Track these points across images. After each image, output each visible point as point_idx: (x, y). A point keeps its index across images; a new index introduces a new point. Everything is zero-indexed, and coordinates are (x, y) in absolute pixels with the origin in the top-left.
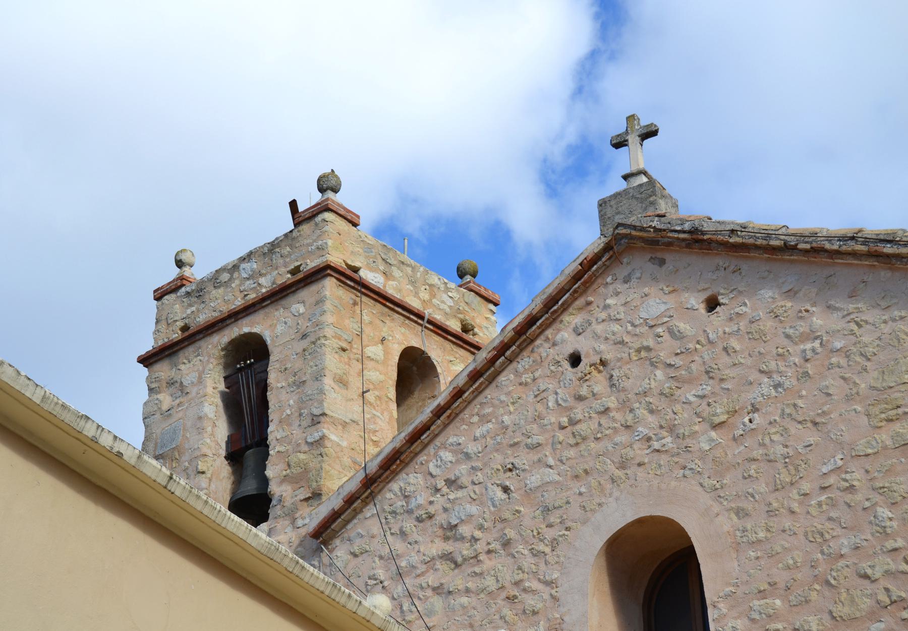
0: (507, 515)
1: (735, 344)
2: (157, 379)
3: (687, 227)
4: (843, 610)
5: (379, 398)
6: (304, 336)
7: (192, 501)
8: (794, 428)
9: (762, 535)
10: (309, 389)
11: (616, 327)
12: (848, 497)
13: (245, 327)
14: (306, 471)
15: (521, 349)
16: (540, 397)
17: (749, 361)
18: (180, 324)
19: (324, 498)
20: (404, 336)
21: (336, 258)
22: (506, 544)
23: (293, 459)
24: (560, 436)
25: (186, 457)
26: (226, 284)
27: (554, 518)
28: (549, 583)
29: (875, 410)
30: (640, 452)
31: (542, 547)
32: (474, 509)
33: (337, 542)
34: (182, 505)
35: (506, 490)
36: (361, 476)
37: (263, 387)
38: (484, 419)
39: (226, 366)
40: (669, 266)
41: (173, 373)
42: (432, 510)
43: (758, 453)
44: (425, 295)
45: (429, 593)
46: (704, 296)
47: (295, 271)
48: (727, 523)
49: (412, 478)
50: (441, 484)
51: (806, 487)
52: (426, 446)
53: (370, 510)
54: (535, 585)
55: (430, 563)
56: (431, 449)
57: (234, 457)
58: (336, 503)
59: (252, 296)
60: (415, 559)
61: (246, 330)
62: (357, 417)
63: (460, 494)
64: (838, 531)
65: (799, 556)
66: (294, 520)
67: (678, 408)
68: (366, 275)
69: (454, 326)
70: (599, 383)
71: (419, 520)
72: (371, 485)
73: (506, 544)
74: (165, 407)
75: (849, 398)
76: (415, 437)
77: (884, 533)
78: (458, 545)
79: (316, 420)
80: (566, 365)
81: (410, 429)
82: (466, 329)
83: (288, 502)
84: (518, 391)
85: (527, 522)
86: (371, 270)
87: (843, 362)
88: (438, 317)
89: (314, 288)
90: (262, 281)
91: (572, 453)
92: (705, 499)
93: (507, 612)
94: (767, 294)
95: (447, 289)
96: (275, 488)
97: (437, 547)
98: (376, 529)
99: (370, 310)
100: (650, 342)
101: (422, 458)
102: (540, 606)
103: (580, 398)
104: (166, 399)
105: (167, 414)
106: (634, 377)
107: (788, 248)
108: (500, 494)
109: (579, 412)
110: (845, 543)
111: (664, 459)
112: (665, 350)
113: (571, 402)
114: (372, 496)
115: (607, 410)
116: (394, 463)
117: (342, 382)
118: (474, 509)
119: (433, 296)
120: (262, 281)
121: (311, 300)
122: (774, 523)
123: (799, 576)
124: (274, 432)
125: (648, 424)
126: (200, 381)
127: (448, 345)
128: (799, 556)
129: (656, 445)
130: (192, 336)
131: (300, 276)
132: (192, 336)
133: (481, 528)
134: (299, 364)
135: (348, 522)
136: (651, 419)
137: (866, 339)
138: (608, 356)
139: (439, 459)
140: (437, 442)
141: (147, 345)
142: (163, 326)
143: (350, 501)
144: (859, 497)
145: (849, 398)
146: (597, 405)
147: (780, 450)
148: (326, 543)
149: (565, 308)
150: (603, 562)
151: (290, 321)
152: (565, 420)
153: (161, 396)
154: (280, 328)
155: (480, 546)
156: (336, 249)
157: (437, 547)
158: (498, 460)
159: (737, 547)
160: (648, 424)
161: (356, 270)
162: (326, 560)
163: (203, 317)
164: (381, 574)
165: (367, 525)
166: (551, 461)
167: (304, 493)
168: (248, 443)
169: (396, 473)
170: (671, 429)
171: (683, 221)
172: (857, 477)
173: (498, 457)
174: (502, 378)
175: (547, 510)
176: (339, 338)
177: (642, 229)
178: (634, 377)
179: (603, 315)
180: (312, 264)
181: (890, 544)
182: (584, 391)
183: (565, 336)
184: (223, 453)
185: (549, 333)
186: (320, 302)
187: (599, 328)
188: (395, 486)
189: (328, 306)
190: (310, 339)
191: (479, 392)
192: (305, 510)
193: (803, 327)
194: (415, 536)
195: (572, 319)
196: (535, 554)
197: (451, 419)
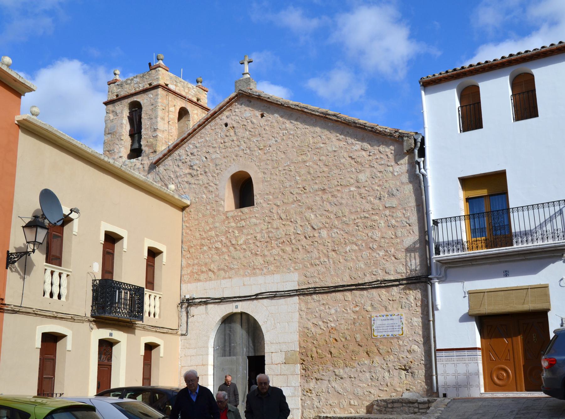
0: (206, 165)
1: (267, 128)
2: (109, 110)
3: (257, 94)
4: (285, 201)
5: (173, 123)
6: (152, 105)
7: (126, 171)
8: (279, 153)
9: (269, 179)
10: (154, 120)
11: (237, 118)
12: (290, 173)
13: (135, 99)
14: (152, 144)
15: (212, 120)
16: (216, 133)
17: (270, 133)
18: (116, 94)
19: (157, 153)
20: (181, 103)
21: (162, 82)
22: (205, 173)
23: (149, 140)
24: (221, 145)
25: (117, 135)
26: (130, 84)
27: (218, 168)
28: (215, 185)
29: (298, 151)
30: (241, 153)
31: (214, 175)
32: (197, 162)
33: (160, 166)
34: (124, 172)
35: (206, 158)
36: (168, 149)
37: (140, 118)
38: (201, 137)
39: (129, 109)
40: (252, 103)
41: (113, 109)
42: (186, 160)
43: (270, 158)
44: (187, 91)
45: (185, 183)
46: (261, 113)
47: (150, 84)
48: (261, 175)
49: (181, 151)
50: (189, 154)
51: (280, 169)
52: (185, 143)
53: (169, 158)
54: (212, 185)
55: (185, 175)
56: (187, 144)
57: (132, 135)
58: (161, 156)
59: (137, 90)
60: (182, 173)
61: (135, 99)
62: (167, 129)
63: (194, 157)
64: (287, 181)
65: (277, 186)
66: (149, 158)
67: (251, 143)
68: (171, 87)
69: (195, 100)
70: (232, 132)
71: (183, 163)
72: (170, 152)
73: (205, 173)
74: (111, 119)
75: (293, 147)
76: (183, 140)
77: (297, 183)
78: (193, 171)
79: (155, 130)
80: (224, 126)
81: (181, 138)
82: (198, 100)
83: (147, 152)
84: (211, 131)
85: (211, 168)
86: (172, 84)
87: (292, 137)
88: (190, 97)
89: (155, 90)
90: (140, 85)
91: (223, 151)
92: (256, 168)
93: (205, 191)
94: (276, 115)
95: (193, 88)
96: (143, 148)
97: (188, 171)
98: (171, 164)
99: (171, 97)
100: (246, 124)
101: (184, 146)
102: (213, 190)
103: (227, 136)
104: (111, 116)
105: (112, 121)
106: (240, 132)
107: (282, 105)
108: (204, 159)
109: (226, 140)
110: (288, 184)
111: (247, 156)
112: (249, 126)
113: (224, 136)
114: (170, 155)
115: (233, 141)
116: (176, 146)
117: (163, 119)
118: (197, 162)
119: (189, 91)
120: (140, 85)
121: (155, 94)
122: (272, 177)
123: (276, 191)
124: (143, 131)
125: (243, 146)
126: (122, 112)
127: (193, 105)
128: (277, 186)
129: (245, 152)
130: (119, 99)
131: (151, 86)
132: (119, 99)
133: (199, 167)
134: (150, 113)
135: (164, 161)
136: (244, 144)
137: (298, 132)
138: (235, 126)
139: (189, 146)
140: (189, 142)
141: (106, 100)
142: (110, 93)
143: (164, 155)
144: (292, 173)
145: (293, 147)
146: (231, 138)
147: (275, 158)
148: (158, 166)
149: (224, 110)
150: (230, 181)
151: (148, 99)
152: (222, 141)
153: (110, 115)
154: (145, 101)
155: (199, 172)
156: (162, 79)
157: (188, 171)
158: (204, 150)
159: (263, 182)
160: (243, 146)
161: (167, 85)
162: (157, 170)
163: (122, 94)
164: (172, 176)
165: (169, 162)
166: (218, 152)
167: (151, 151)
168: (136, 132)
169: (177, 149)
170: (249, 148)
171: (256, 92)
172: (292, 168)
173: (205, 149)
174: (207, 127)
175: (216, 165)
176: (162, 106)
177: (246, 92)
178: (240, 132)
179: (234, 114)
180: (155, 83)
181: (298, 186)
182: (228, 134)
183: (224, 117)
184: (128, 134)
185: (220, 116)
186: (157, 95)
187: (233, 117)
188: (177, 152)
189: (159, 97)
190: (154, 106)
191: (200, 130)
192: (152, 155)
193: (284, 126)
194: (182, 167)
195: (226, 113)
196: (213, 176)
197: (192, 136)
